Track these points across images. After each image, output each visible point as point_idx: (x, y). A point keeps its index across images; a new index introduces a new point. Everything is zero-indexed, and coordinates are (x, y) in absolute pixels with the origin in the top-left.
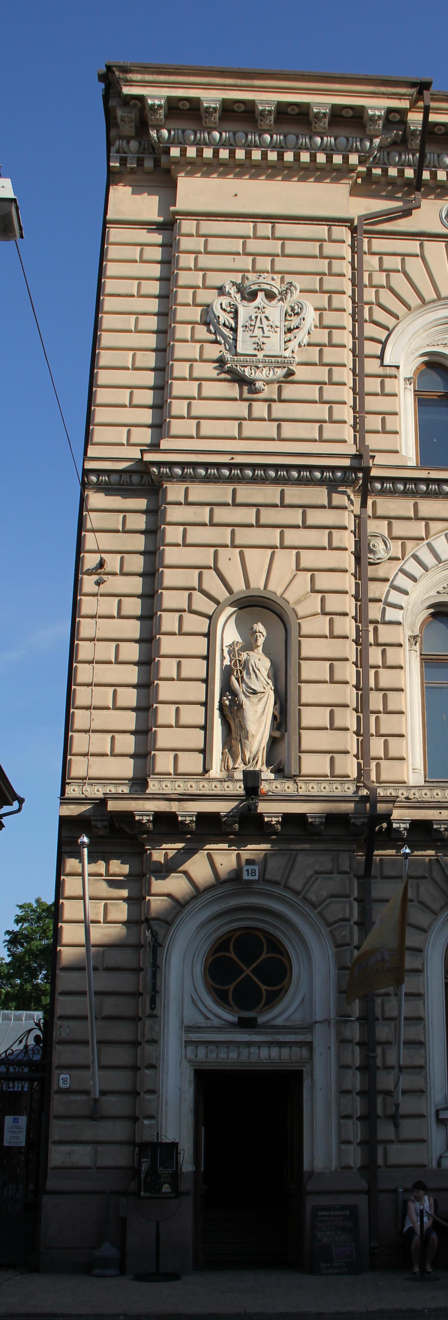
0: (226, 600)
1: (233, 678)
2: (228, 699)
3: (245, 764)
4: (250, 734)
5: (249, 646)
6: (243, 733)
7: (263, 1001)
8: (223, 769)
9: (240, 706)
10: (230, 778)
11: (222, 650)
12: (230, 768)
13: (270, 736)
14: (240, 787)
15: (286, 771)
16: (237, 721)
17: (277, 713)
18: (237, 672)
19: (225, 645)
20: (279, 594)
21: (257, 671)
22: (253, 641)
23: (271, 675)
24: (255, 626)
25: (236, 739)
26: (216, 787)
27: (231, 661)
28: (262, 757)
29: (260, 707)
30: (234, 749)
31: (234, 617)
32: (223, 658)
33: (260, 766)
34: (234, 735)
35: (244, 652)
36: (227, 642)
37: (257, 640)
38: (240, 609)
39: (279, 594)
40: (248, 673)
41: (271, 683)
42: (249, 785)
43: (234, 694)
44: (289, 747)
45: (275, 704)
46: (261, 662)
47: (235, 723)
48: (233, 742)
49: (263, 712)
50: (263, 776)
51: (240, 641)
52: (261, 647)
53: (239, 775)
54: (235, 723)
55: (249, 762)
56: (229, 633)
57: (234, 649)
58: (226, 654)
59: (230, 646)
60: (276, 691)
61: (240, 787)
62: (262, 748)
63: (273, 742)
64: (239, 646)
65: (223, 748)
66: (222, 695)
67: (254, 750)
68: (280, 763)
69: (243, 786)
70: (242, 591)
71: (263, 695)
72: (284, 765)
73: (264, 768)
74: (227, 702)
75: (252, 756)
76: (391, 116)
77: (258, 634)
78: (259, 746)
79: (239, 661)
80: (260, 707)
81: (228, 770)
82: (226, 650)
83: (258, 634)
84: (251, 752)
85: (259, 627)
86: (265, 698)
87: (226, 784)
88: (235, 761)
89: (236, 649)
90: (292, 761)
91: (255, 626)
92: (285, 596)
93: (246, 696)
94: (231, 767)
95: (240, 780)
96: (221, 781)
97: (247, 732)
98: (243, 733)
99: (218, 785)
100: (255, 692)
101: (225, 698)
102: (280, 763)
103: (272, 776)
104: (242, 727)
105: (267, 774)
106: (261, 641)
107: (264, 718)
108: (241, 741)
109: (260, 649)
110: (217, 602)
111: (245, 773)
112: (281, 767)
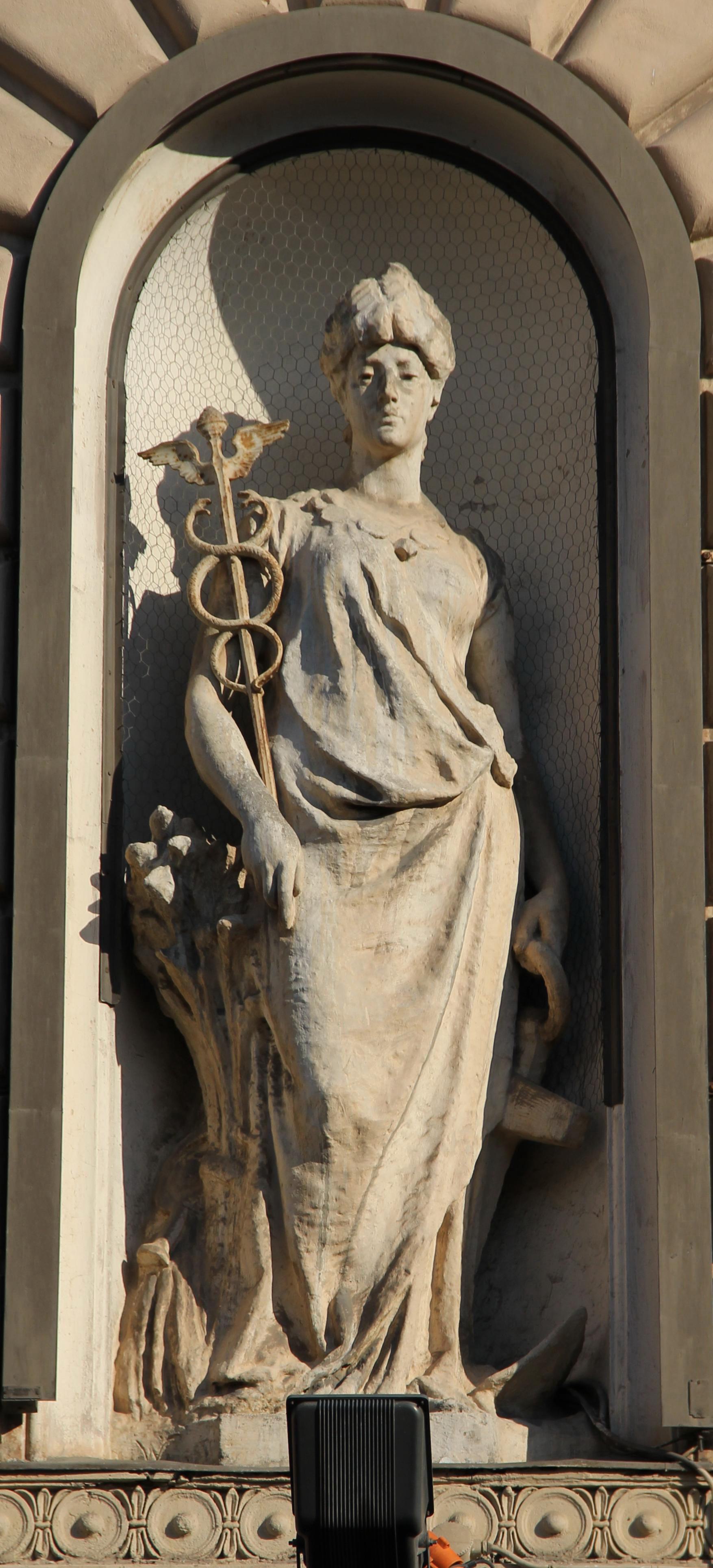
0: (142, 91)
1: (205, 697)
2: (167, 854)
3: (305, 1350)
4: (338, 1123)
5: (325, 448)
6: (286, 1117)
7: (279, 641)
8: (135, 1390)
9: (264, 911)
10: (193, 1462)
11: (120, 480)
12: (193, 1383)
13: (495, 1135)
14: (268, 1531)
15: (619, 1403)
16: (238, 1021)
17: (539, 960)
18: (235, 645)
19: (139, 438)
20: (543, 43)
21: (375, 627)
22: (351, 410)
23: (492, 670)
24: (367, 295)
25: (236, 1161)
26: (80, 1530)
27: (183, 567)
28: (431, 1297)
29: (415, 912)
30: (217, 1235)
31: (201, 226)
32: (124, 545)
33: (422, 1361)
34: (217, 1131)
35: (283, 494)
36: (154, 420)
37: (378, 402)
38: (247, 162)
39: (543, 43)
40: (322, 661)
41: (494, 734)
42: (340, 1510)
43: (219, 819)
44: (640, 1215)
45: (529, 887)
46: (414, 573)
47: (224, 1038)
48: (214, 1182)
49: (436, 957)
50: (448, 1444)
51: (253, 408)
52: (416, 457)
53: (257, 1438)
54: (224, 1038)
55: (335, 1338)
56: (158, 354)
57: (207, 475)
58: (146, 515)
59: (179, 448)
60: (534, 794)
61: (268, 1531)
62: (433, 1222)
63: (519, 1181)
64: (250, 448)
65: (138, 1232)
66: (120, 828)
67: (373, 1243)
68: (573, 1339)
69: (287, 1524)
70: (263, 25)
71: (433, 819)
72: (601, 1359)
73: (451, 1380)
74: (162, 881)
75: (358, 1286)
76: (147, 890)
77: (388, 356)
78: (412, 1213)
79: (252, 562)
80: (415, 912)
81: (172, 1397)
82: (145, 480)
83: (388, 356)
84: (346, 1262)
85: (401, 302)
86: (451, 847)
87: (162, 1507)
88: (224, 1328)
89: (228, 470)
90: (668, 1320)
91: (367, 295)
92: (596, 54)
93: (310, 835)
94: (196, 1375)
95: (261, 1478)
96: (123, 1483)
97: (317, 1107)
98: (286, 1117)
99: (101, 1513)
100: (372, 803)
101: (148, 849)
102: (573, 1339)
103: (512, 1441)
104: (281, 1069)
105: (475, 1428)
106: (412, 408)
107: (444, 996)
108: (268, 1175)
109: (408, 470)
110: (69, 110)
111: (306, 1419)
112: (580, 1370)
